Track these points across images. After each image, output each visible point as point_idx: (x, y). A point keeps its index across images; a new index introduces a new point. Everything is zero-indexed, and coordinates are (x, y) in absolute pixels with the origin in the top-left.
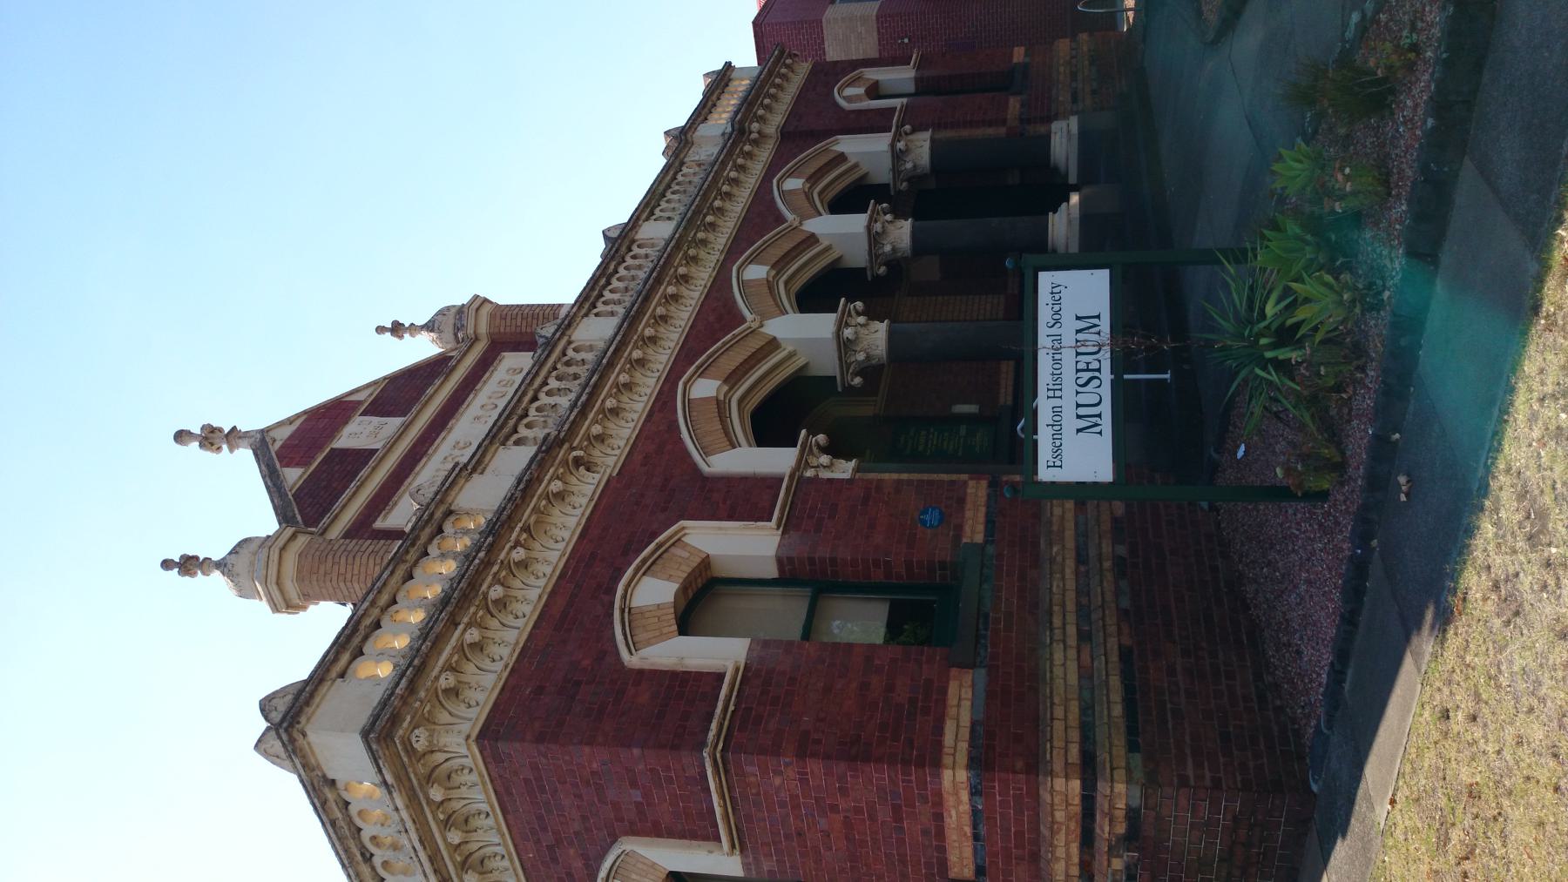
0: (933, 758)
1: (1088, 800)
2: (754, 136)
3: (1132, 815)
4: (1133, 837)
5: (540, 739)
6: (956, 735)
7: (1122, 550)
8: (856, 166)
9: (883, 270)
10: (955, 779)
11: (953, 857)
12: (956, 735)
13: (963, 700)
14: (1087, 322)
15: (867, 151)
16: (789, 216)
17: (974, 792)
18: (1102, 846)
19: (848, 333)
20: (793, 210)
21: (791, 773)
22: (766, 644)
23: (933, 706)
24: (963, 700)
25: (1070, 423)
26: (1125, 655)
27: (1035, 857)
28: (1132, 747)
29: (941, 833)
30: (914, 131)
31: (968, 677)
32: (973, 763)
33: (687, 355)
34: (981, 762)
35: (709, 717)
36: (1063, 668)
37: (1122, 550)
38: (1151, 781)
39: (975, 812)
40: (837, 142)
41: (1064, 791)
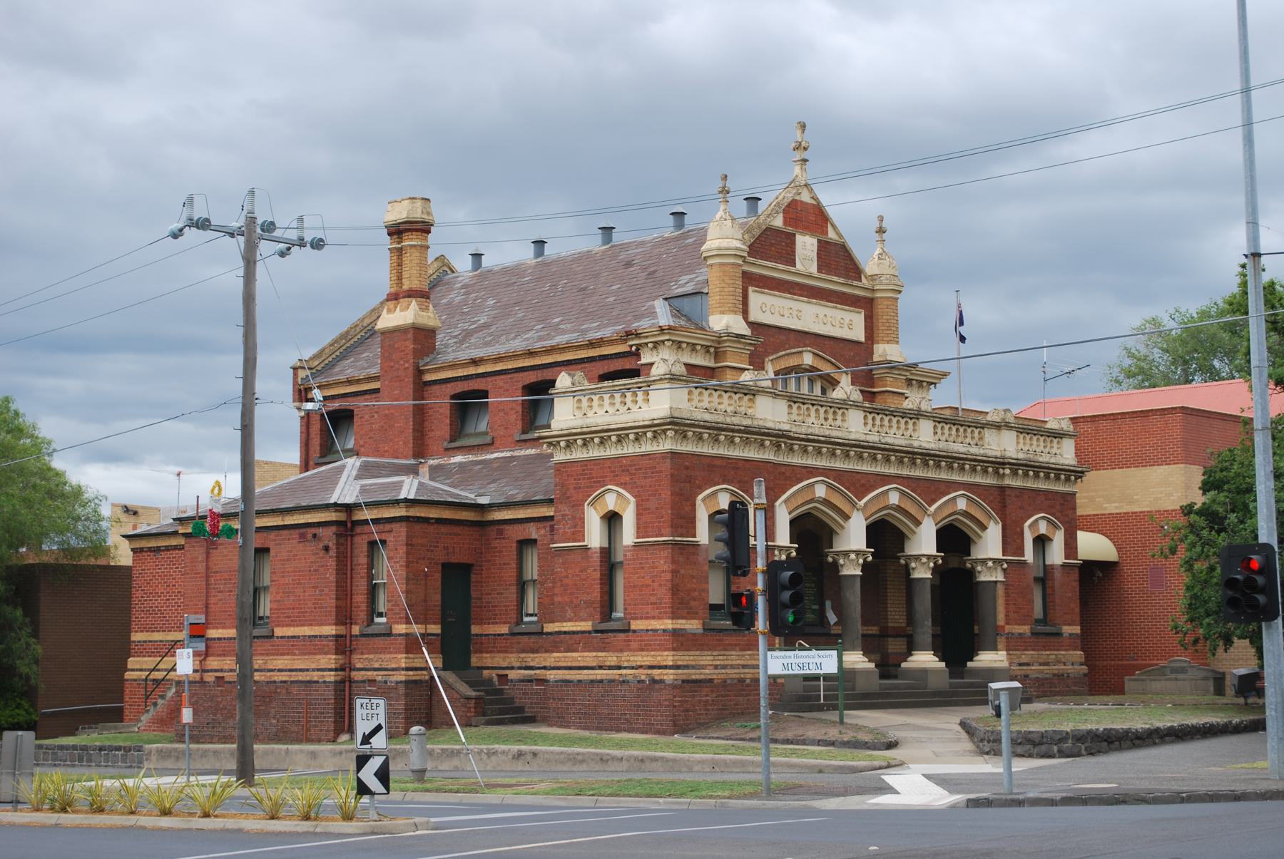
0: (674, 616)
1: (666, 667)
2: (1001, 471)
3: (662, 681)
4: (654, 681)
5: (672, 475)
6: (682, 624)
7: (748, 681)
8: (843, 527)
9: (830, 559)
10: (668, 624)
11: (639, 622)
12: (682, 624)
13: (693, 625)
14: (819, 666)
15: (990, 544)
16: (933, 508)
17: (664, 631)
18: (650, 672)
19: (853, 556)
20: (866, 504)
21: (666, 567)
22: (707, 550)
23: (690, 615)
24: (693, 625)
25: (786, 661)
26: (711, 680)
27: (642, 650)
28: (683, 681)
29: (647, 618)
30: (1004, 570)
31: (700, 626)
32: (674, 630)
33: (839, 475)
34: (675, 633)
35: (681, 536)
36: (706, 658)
37: (748, 681)
38: (674, 687)
39: (656, 631)
40: (996, 523)
41: (668, 658)
